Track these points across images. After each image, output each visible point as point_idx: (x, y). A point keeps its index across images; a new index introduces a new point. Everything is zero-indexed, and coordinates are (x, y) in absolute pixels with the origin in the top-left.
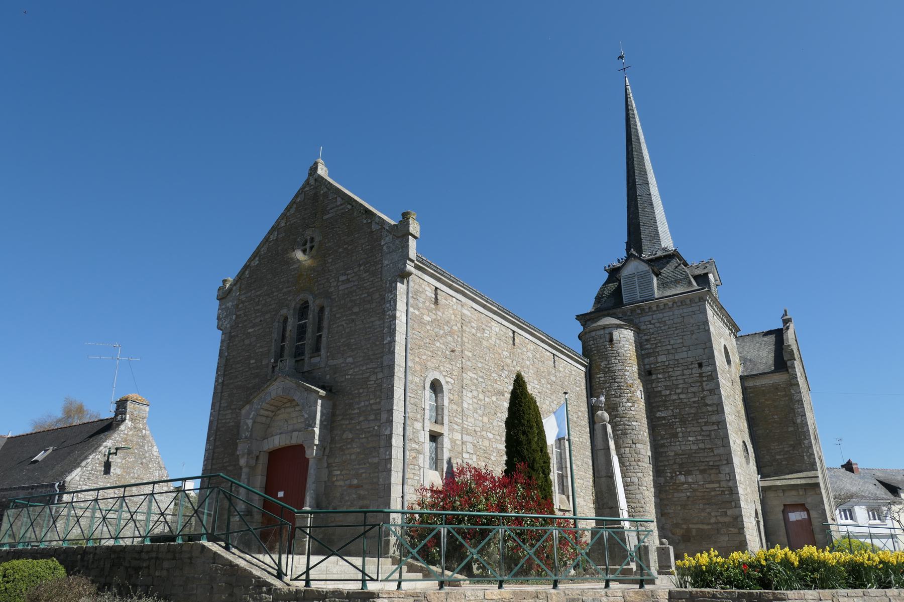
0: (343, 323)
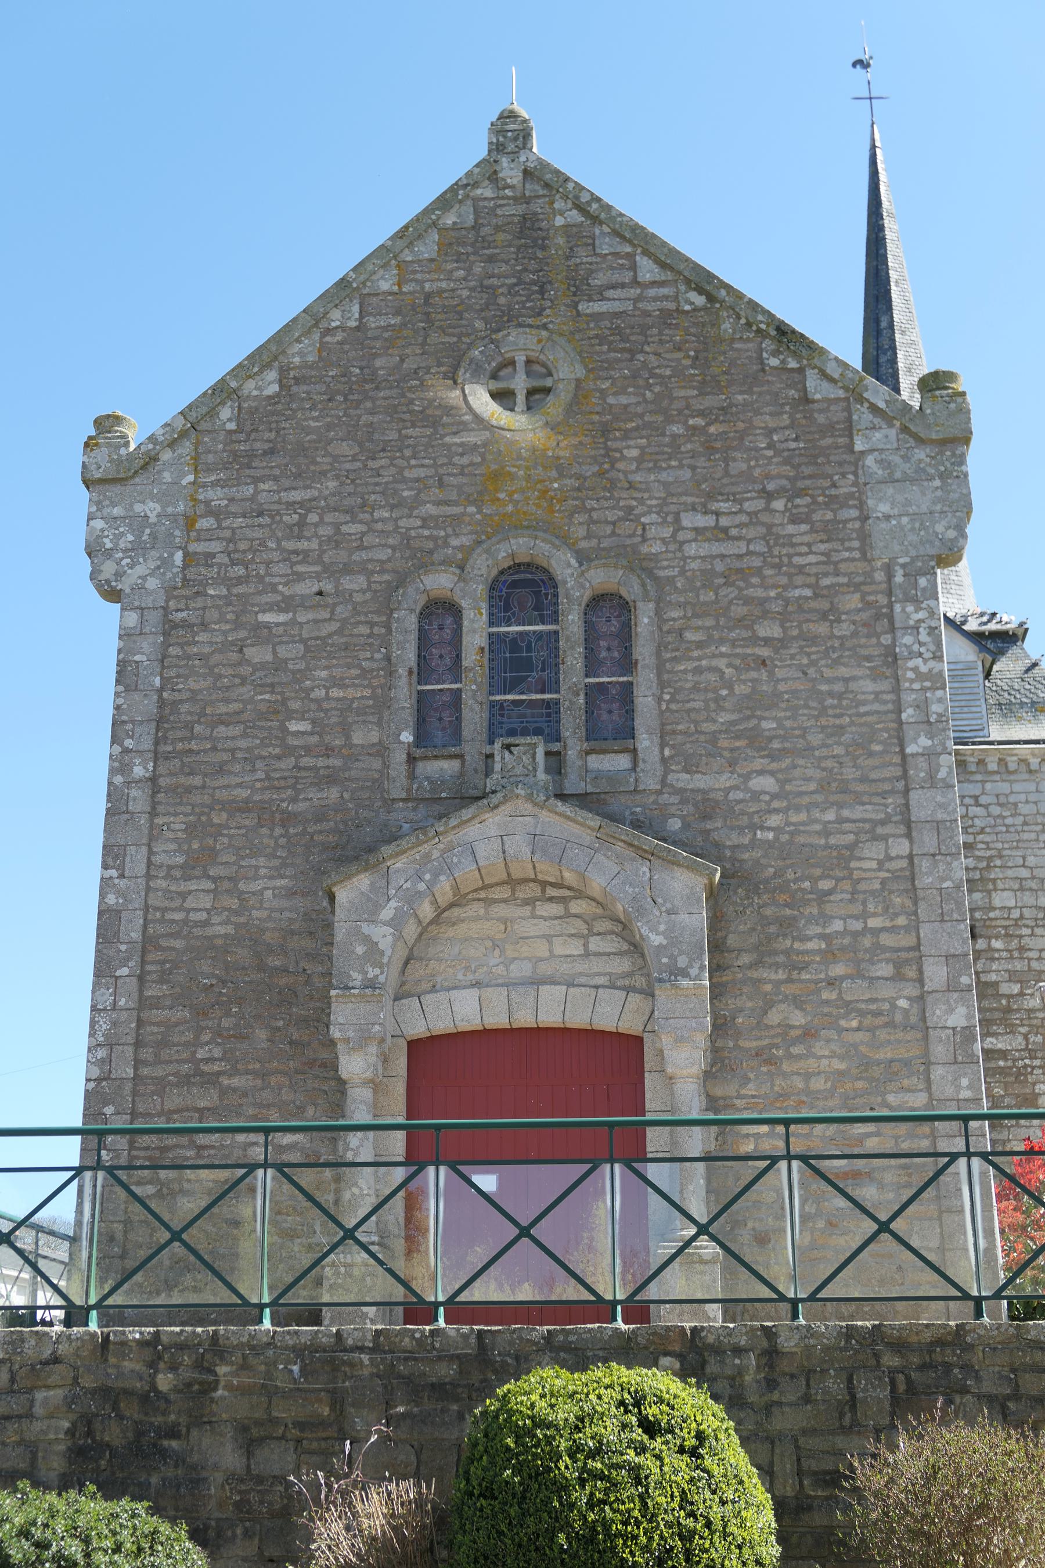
0: (721, 663)
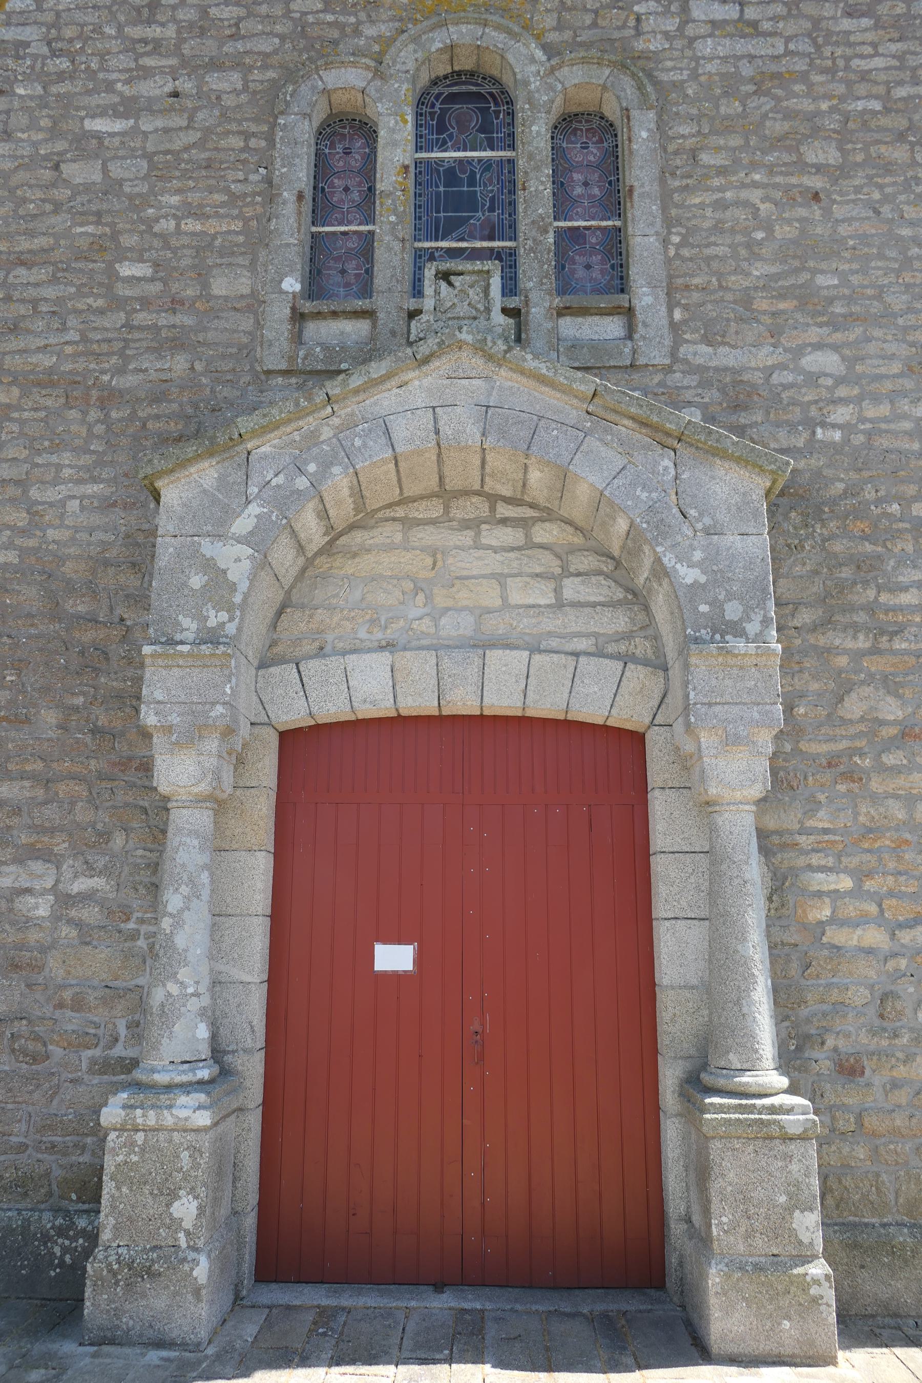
0: (755, 196)
